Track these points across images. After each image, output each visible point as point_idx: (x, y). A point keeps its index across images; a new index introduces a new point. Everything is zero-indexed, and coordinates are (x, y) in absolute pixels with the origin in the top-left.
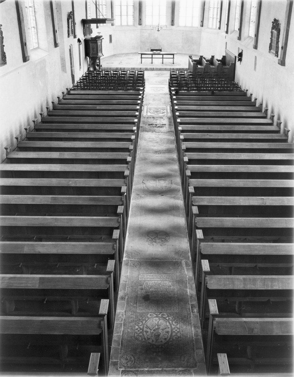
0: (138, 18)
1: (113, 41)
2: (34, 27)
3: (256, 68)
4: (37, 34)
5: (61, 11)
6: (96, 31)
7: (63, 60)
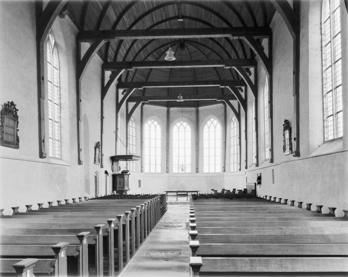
0: (166, 166)
1: (141, 186)
2: (58, 140)
3: (274, 181)
4: (61, 147)
5: (88, 137)
7: (87, 181)
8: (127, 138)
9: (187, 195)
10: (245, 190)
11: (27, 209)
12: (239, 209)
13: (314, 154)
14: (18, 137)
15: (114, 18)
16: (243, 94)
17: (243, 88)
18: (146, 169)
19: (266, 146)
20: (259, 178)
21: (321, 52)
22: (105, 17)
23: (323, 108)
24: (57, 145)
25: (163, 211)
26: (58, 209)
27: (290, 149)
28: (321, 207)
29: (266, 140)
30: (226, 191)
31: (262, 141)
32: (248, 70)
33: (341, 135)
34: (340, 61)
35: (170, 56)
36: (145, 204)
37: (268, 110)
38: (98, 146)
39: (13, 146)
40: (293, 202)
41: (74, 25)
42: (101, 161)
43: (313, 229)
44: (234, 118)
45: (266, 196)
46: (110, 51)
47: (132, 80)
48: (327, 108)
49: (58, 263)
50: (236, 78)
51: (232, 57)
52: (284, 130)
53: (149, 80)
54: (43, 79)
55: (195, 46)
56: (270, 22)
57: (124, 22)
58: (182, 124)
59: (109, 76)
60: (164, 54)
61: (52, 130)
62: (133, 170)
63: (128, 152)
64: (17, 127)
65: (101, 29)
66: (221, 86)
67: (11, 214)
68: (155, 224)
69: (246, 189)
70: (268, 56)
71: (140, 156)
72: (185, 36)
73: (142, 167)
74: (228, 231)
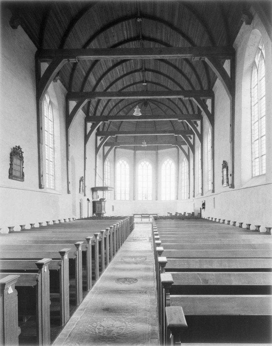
1: (114, 210)
2: (52, 175)
6: (100, 194)
7: (74, 206)
8: (103, 174)
9: (149, 217)
10: (193, 213)
11: (31, 227)
12: (189, 227)
13: (245, 186)
14: (24, 173)
15: (94, 82)
16: (192, 141)
17: (192, 136)
18: (118, 197)
19: (209, 180)
20: (204, 204)
21: (250, 110)
22: (87, 82)
23: (252, 152)
24: (51, 179)
25: (132, 229)
26: (53, 226)
27: (227, 182)
28: (249, 225)
29: (209, 175)
30: (179, 214)
31: (206, 177)
32: (196, 123)
33: (264, 172)
34: (265, 117)
35: (137, 112)
36: (120, 223)
37: (210, 153)
38: (82, 180)
39: (20, 179)
40: (229, 221)
41: (64, 87)
42: (84, 191)
43: (244, 240)
44: (185, 159)
45: (209, 218)
46: (91, 107)
47: (108, 129)
48: (254, 152)
49: (63, 262)
50: (186, 129)
51: (184, 113)
52: (223, 168)
53: (120, 130)
54: (42, 129)
55: (155, 104)
56: (213, 87)
57: (102, 85)
58: (145, 163)
59: (90, 126)
60: (132, 109)
61: (48, 168)
62: (108, 198)
63: (104, 184)
64: (23, 165)
65: (84, 91)
66: (175, 134)
67: (20, 230)
68: (126, 238)
69: (194, 213)
70: (211, 112)
71: (113, 187)
72: (149, 97)
73: (115, 196)
74: (182, 242)
